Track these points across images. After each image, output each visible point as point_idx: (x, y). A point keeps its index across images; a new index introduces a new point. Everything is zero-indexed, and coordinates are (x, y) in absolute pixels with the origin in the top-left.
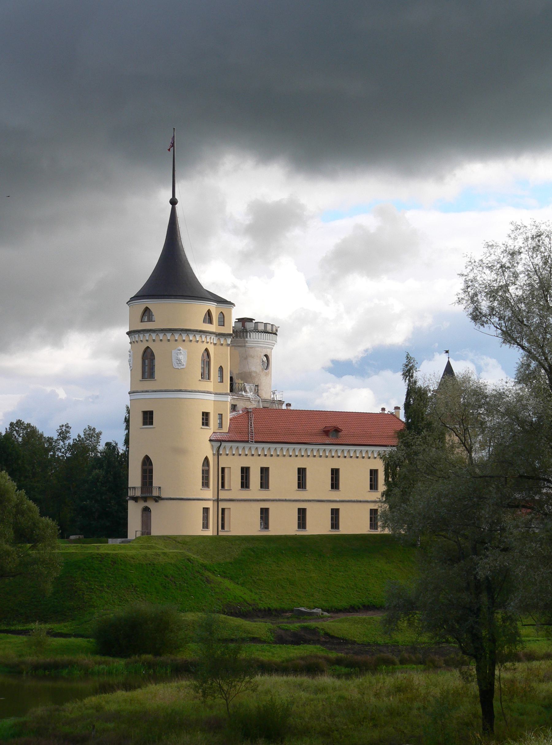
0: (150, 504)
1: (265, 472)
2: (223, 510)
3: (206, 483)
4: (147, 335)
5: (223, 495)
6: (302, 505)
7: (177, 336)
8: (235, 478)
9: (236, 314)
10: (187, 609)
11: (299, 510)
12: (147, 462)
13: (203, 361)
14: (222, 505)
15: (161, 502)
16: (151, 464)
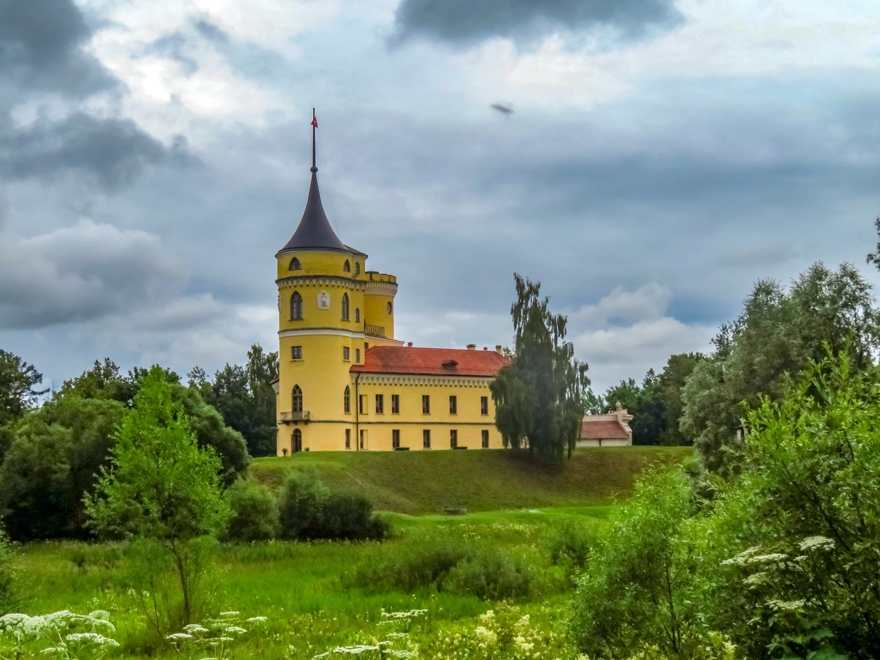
0: (300, 427)
1: (395, 398)
2: (362, 431)
3: (347, 409)
4: (295, 282)
5: (361, 418)
6: (396, 427)
7: (314, 282)
8: (370, 405)
9: (368, 266)
10: (700, 607)
11: (394, 431)
12: (297, 390)
13: (343, 302)
14: (361, 427)
15: (310, 425)
16: (300, 392)
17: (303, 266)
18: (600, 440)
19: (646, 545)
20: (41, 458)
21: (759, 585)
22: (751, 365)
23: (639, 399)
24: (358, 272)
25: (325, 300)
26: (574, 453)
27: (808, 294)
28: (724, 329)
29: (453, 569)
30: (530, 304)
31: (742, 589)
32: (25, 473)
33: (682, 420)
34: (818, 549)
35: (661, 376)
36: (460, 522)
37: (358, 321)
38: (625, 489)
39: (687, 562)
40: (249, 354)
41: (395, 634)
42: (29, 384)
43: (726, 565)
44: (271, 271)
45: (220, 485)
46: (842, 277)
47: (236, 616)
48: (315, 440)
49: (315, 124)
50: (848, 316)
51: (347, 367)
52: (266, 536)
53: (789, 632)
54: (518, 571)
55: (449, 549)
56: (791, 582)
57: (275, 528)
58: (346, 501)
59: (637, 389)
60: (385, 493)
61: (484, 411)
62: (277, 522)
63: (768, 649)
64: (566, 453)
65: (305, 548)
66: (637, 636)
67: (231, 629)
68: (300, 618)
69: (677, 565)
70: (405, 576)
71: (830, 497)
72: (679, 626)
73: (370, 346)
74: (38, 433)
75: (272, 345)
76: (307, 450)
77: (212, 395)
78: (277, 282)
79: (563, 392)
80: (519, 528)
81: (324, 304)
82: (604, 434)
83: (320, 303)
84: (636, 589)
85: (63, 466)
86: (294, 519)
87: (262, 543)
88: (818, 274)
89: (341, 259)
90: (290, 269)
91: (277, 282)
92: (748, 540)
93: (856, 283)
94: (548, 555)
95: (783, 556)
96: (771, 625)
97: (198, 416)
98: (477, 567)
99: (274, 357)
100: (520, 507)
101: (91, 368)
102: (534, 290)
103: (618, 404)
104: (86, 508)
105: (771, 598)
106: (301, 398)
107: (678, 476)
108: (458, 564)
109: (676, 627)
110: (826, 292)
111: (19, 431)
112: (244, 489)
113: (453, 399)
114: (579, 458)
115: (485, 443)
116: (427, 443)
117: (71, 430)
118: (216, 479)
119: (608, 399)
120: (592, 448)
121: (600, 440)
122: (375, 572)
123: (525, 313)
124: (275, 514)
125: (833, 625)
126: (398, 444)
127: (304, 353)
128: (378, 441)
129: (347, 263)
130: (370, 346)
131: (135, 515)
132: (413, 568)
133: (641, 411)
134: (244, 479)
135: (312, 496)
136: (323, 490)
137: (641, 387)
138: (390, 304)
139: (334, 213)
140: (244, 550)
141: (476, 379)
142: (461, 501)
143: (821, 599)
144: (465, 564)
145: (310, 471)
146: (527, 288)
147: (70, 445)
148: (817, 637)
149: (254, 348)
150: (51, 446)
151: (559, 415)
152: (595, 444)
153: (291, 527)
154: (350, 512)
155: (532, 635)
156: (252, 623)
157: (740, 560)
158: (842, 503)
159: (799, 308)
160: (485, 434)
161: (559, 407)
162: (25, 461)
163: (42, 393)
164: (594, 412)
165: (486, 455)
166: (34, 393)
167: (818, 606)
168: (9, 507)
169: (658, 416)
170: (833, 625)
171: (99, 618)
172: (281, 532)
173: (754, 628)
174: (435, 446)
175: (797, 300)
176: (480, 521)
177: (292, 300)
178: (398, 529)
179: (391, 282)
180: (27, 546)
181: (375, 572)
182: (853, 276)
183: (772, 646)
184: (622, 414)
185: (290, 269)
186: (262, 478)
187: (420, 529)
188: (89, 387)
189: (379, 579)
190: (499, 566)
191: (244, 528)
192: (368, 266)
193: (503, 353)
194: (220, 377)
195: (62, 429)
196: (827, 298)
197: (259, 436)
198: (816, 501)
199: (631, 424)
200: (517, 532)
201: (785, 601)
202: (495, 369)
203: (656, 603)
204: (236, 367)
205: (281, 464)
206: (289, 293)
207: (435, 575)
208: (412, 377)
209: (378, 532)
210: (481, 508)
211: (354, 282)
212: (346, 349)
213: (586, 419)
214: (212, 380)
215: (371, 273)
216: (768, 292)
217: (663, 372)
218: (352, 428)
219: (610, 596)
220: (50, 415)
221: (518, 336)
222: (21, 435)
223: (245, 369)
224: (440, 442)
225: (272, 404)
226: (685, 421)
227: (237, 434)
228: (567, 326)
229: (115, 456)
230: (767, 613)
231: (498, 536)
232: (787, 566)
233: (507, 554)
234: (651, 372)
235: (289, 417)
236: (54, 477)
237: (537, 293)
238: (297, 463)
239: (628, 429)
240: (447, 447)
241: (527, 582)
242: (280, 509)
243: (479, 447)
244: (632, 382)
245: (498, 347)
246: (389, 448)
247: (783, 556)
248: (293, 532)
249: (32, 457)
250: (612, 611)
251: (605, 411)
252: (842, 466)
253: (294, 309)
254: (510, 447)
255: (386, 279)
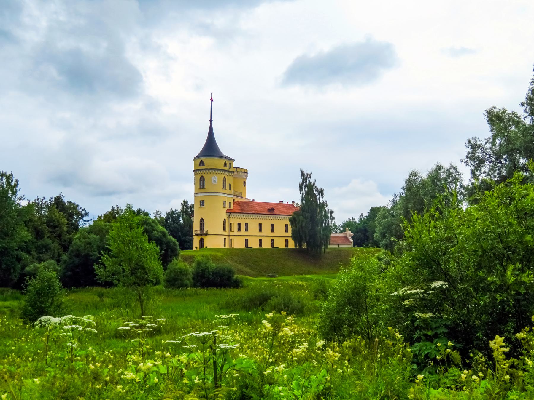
0: (203, 237)
1: (246, 225)
3: (225, 229)
5: (231, 233)
6: (247, 238)
7: (210, 171)
8: (235, 227)
9: (235, 165)
14: (231, 237)
15: (208, 236)
17: (205, 164)
18: (339, 245)
19: (356, 288)
20: (85, 249)
21: (410, 305)
22: (407, 208)
23: (357, 226)
24: (230, 167)
25: (215, 180)
26: (327, 250)
27: (435, 176)
28: (395, 196)
29: (269, 301)
30: (308, 183)
31: (401, 308)
32: (78, 256)
33: (375, 234)
34: (440, 287)
35: (366, 216)
36: (274, 281)
37: (230, 189)
38: (347, 263)
39: (375, 296)
40: (182, 204)
41: (222, 326)
42: (83, 217)
43: (393, 296)
44: (191, 166)
45: (159, 259)
46: (450, 168)
47: (150, 318)
48: (211, 243)
49: (212, 99)
50: (452, 187)
51: (225, 210)
52: (186, 286)
53: (424, 329)
54: (299, 302)
55: (268, 292)
56: (425, 304)
57: (190, 282)
58: (223, 270)
59: (356, 222)
60: (241, 267)
61: (287, 231)
62: (191, 279)
63: (414, 337)
64: (323, 250)
65: (204, 291)
66: (351, 332)
67: (149, 325)
68: (196, 322)
69: (370, 297)
70: (247, 304)
71: (445, 263)
72: (371, 327)
73: (235, 201)
74: (84, 238)
75: (191, 201)
76: (206, 247)
77: (164, 222)
78: (194, 171)
79: (322, 223)
80: (299, 283)
81: (215, 181)
82: (340, 241)
83: (213, 181)
84: (350, 309)
85: (95, 253)
86: (199, 278)
87: (184, 289)
88: (439, 168)
89: (223, 161)
90: (200, 165)
91: (194, 171)
92: (404, 283)
93: (457, 172)
94: (313, 295)
95: (422, 291)
96: (416, 325)
97: (157, 231)
98: (280, 300)
99: (192, 206)
100: (302, 274)
101: (110, 210)
102: (309, 176)
103: (347, 228)
104: (95, 271)
105: (416, 312)
106: (204, 224)
107: (374, 260)
108: (272, 298)
109: (369, 327)
110: (442, 176)
111: (75, 237)
112: (177, 264)
113: (272, 225)
114: (329, 253)
115: (287, 245)
116: (260, 245)
117: (99, 237)
118: (157, 256)
119: (343, 227)
120: (335, 248)
121: (339, 245)
122: (233, 302)
123: (305, 186)
124: (190, 276)
125: (446, 326)
126: (247, 245)
127: (205, 204)
128: (238, 244)
129: (225, 163)
130: (235, 201)
131: (118, 273)
132: (251, 300)
133: (357, 232)
134: (177, 259)
135: (207, 268)
136: (213, 265)
137: (358, 222)
138: (245, 182)
139: (224, 146)
140: (176, 292)
141: (283, 216)
142: (275, 271)
143: (440, 314)
144: (275, 299)
145: (207, 256)
146: (306, 175)
147: (98, 243)
148: (438, 332)
149: (184, 201)
150: (90, 244)
151: (320, 233)
152: (336, 246)
153: (198, 282)
154: (224, 275)
155: (302, 331)
156: (159, 322)
157: (401, 293)
158: (452, 265)
159: (430, 183)
160: (287, 241)
161: (320, 229)
162: (78, 250)
163: (88, 221)
164: (336, 232)
165: (287, 251)
166: (85, 221)
167: (438, 317)
168: (70, 271)
169: (365, 235)
170: (446, 326)
171: (88, 319)
172: (193, 284)
173: (407, 327)
174: (264, 247)
175: (429, 180)
176: (283, 280)
177: (200, 180)
178: (246, 283)
179: (245, 172)
180: (78, 289)
181: (233, 302)
182: (455, 168)
183: (416, 336)
184: (349, 233)
185: (200, 165)
186: (185, 259)
187: (256, 283)
188: (109, 218)
189: (235, 305)
190: (290, 300)
191: (175, 282)
192: (235, 165)
193: (296, 205)
194: (168, 214)
195: (95, 236)
196: (442, 179)
197: (185, 241)
198: (439, 265)
199: (353, 237)
200: (300, 285)
201: (423, 313)
202: (291, 212)
203: (360, 316)
204: (176, 210)
205: (194, 254)
206: (199, 176)
207: (260, 304)
208: (254, 215)
209: (237, 284)
210: (284, 274)
211: (229, 172)
212: (225, 202)
213: (332, 235)
214: (164, 216)
215: (236, 168)
216: (416, 175)
217: (367, 215)
218: (227, 238)
219: (338, 312)
220: (92, 230)
221: (302, 197)
222: (76, 239)
223: (179, 211)
224: (267, 245)
225: (191, 227)
226: (377, 235)
227: (174, 240)
228: (324, 192)
229: (109, 245)
230: (414, 319)
231: (291, 287)
232: (424, 296)
233: (293, 294)
234: (362, 215)
235: (199, 232)
236: (91, 258)
237: (310, 177)
238: (201, 253)
239: (351, 240)
240: (269, 247)
241: (303, 307)
242: (193, 273)
243: (284, 247)
244: (353, 219)
245: (293, 202)
246: (243, 247)
247: (422, 291)
248: (198, 284)
249: (81, 248)
250: (338, 319)
251: (341, 232)
252: (452, 247)
253: (201, 183)
254: (298, 247)
255: (243, 171)
